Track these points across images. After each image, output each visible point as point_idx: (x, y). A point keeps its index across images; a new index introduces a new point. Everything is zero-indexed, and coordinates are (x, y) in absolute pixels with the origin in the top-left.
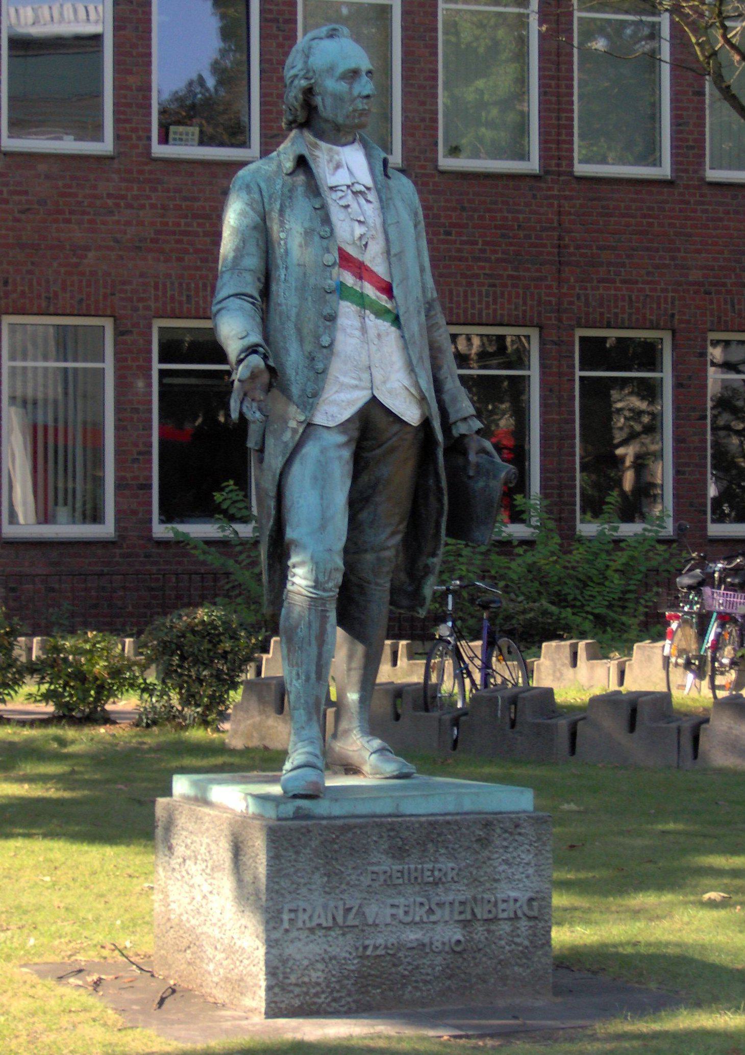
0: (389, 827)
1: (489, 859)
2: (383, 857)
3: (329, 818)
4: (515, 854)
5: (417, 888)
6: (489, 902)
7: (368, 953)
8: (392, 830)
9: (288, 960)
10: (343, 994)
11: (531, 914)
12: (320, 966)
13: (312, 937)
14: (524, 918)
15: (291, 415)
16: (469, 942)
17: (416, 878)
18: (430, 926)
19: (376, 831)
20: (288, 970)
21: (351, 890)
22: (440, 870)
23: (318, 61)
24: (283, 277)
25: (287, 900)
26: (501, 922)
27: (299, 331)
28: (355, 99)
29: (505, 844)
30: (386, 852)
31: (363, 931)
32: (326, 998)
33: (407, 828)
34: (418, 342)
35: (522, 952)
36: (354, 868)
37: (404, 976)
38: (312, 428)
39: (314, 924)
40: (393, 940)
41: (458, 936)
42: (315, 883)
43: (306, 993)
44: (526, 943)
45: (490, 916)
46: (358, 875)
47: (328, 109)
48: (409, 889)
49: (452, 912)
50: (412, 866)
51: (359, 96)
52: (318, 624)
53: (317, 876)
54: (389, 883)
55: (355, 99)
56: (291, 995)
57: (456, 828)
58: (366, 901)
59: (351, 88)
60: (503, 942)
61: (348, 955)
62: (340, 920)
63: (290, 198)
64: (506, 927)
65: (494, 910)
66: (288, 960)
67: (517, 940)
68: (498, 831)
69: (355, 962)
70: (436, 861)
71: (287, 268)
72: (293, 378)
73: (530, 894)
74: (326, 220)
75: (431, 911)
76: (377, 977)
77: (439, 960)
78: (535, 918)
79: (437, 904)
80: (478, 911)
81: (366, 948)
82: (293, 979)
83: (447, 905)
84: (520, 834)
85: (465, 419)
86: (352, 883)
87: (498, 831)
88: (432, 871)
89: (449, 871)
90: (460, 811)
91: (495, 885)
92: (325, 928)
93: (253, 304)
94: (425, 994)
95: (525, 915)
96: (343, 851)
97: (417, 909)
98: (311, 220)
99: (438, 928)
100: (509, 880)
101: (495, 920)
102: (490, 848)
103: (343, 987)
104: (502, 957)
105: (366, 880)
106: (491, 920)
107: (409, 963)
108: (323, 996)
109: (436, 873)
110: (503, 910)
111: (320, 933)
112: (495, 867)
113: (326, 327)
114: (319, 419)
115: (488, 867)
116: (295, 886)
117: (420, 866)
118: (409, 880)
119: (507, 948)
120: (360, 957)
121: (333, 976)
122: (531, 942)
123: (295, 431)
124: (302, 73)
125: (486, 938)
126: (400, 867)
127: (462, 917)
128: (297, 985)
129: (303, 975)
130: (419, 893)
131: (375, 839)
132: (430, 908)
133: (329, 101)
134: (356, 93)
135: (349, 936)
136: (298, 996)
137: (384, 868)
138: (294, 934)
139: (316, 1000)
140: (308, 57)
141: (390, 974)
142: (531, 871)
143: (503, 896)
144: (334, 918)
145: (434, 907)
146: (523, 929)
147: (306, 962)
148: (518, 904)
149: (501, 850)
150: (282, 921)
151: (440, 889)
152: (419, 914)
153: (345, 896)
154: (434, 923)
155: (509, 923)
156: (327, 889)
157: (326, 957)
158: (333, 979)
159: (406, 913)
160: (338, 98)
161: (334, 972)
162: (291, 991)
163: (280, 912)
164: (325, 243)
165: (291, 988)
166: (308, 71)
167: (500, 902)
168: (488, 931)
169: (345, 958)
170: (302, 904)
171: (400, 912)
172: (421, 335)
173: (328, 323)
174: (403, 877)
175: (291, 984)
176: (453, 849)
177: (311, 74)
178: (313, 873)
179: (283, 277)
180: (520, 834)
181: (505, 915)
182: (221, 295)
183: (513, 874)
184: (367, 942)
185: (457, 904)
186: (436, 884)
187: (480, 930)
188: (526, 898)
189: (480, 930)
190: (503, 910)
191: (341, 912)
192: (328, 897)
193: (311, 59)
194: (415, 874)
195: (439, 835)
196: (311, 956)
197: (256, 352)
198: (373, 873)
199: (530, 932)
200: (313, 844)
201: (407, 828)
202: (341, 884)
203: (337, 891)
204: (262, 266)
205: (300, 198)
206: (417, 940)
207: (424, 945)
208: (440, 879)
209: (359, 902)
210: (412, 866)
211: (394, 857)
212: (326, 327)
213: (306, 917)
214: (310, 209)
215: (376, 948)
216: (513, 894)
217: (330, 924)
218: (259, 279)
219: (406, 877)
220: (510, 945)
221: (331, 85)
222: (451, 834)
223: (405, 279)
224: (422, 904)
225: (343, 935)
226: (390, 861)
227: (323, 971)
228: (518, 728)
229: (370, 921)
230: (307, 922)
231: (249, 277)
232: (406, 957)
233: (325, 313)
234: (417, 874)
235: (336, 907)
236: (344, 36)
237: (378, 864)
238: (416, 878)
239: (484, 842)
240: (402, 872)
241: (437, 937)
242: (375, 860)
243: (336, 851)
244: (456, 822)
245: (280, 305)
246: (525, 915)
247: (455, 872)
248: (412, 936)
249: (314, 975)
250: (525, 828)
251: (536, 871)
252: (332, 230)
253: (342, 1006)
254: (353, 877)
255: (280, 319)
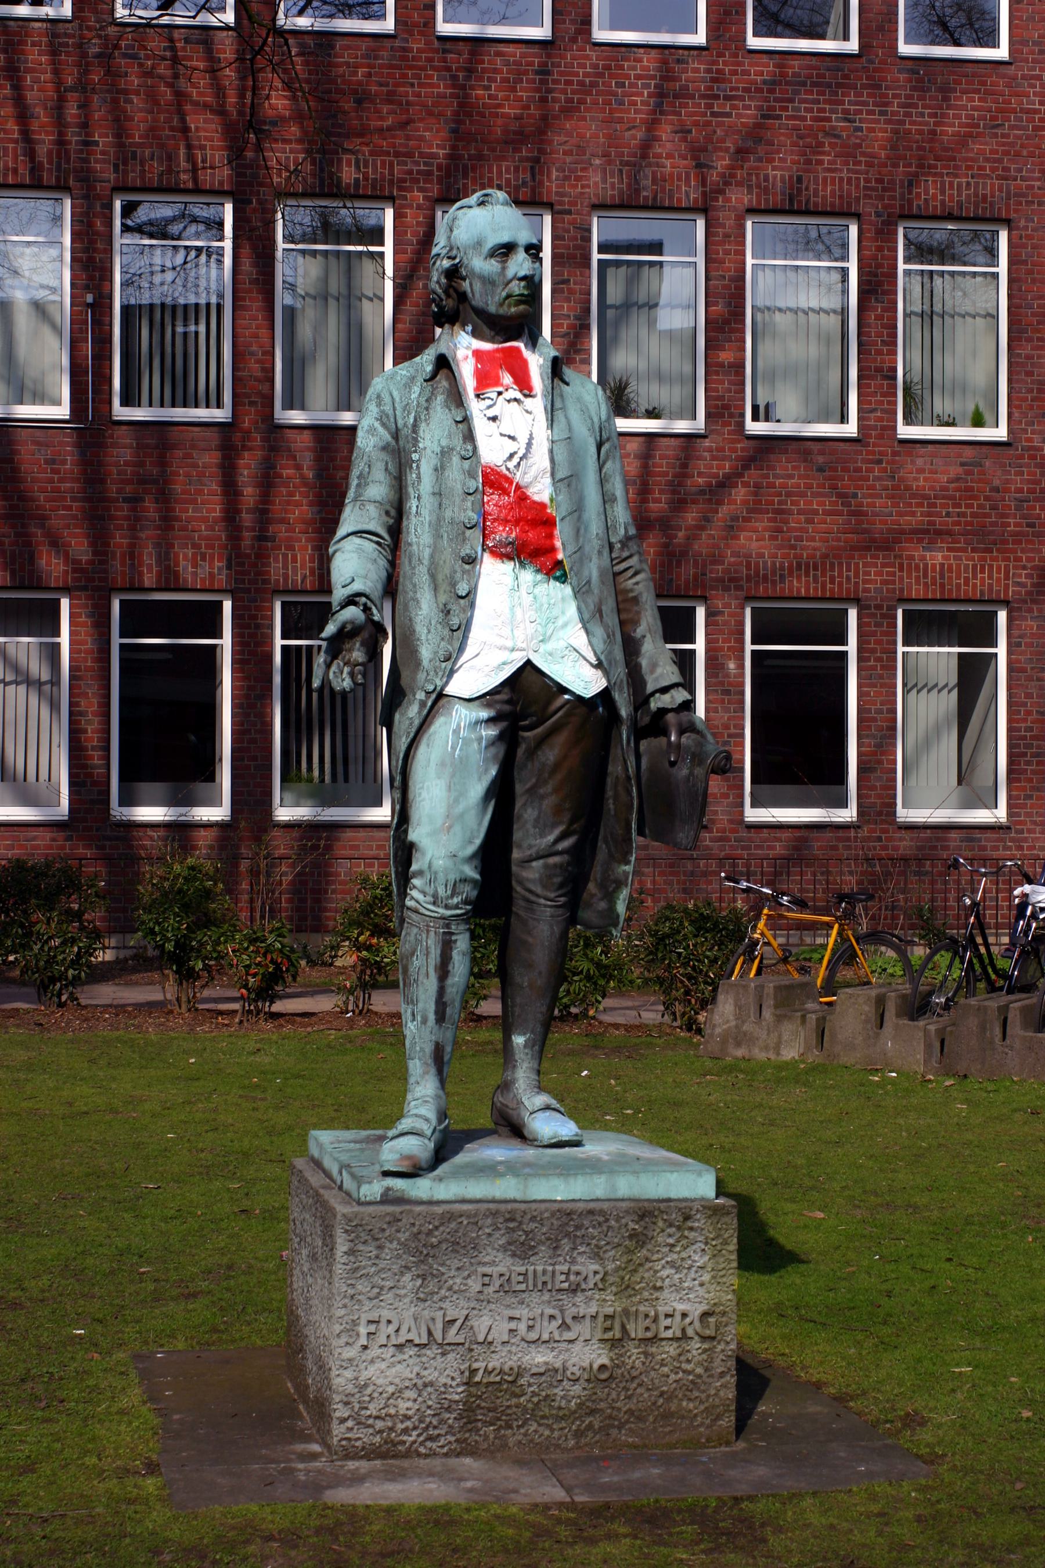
0: (507, 1216)
1: (647, 1260)
2: (500, 1255)
3: (430, 1203)
4: (684, 1255)
5: (546, 1296)
6: (647, 1316)
7: (477, 1379)
8: (512, 1220)
9: (366, 1386)
10: (443, 1432)
11: (708, 1332)
12: (412, 1394)
13: (400, 1357)
14: (696, 1338)
15: (420, 684)
16: (618, 1366)
17: (545, 1283)
18: (564, 1345)
19: (489, 1221)
20: (367, 1399)
21: (455, 1296)
22: (578, 1273)
23: (463, 234)
24: (414, 509)
25: (366, 1308)
26: (664, 1343)
27: (433, 577)
28: (511, 281)
29: (671, 1241)
30: (504, 1248)
31: (471, 1350)
32: (419, 1435)
33: (533, 1219)
34: (596, 591)
35: (692, 1382)
36: (458, 1269)
37: (525, 1410)
38: (444, 701)
39: (401, 1340)
40: (511, 1363)
41: (604, 1360)
42: (404, 1287)
43: (391, 1429)
44: (699, 1370)
45: (649, 1335)
46: (466, 1278)
47: (477, 295)
48: (535, 1298)
49: (593, 1329)
50: (540, 1268)
51: (515, 278)
52: (439, 952)
53: (408, 1277)
54: (506, 1289)
55: (511, 281)
56: (371, 1431)
57: (601, 1219)
58: (475, 1312)
59: (504, 269)
60: (666, 1369)
61: (449, 1382)
62: (438, 1335)
63: (427, 409)
64: (672, 1349)
65: (653, 1327)
66: (366, 1386)
67: (686, 1366)
68: (661, 1224)
69: (460, 1390)
70: (573, 1262)
71: (419, 498)
72: (423, 637)
73: (703, 1308)
74: (469, 436)
75: (565, 1326)
76: (489, 1410)
77: (577, 1389)
78: (713, 1338)
79: (574, 1318)
80: (630, 1327)
81: (473, 1372)
82: (373, 1409)
83: (588, 1320)
84: (691, 1229)
85: (664, 690)
86: (456, 1288)
87: (661, 1224)
88: (568, 1274)
89: (591, 1275)
90: (613, 1196)
91: (656, 1295)
92: (417, 1345)
93: (378, 543)
94: (556, 1434)
95: (697, 1334)
96: (444, 1246)
97: (545, 1323)
98: (450, 436)
99: (577, 1348)
100: (677, 1288)
101: (655, 1339)
102: (649, 1246)
103: (442, 1422)
104: (665, 1388)
105: (475, 1285)
106: (649, 1339)
107: (534, 1393)
108: (415, 1433)
109: (572, 1277)
110: (667, 1328)
111: (411, 1351)
112: (656, 1272)
113: (464, 572)
114: (449, 690)
115: (648, 1270)
116: (376, 1290)
117: (550, 1268)
118: (535, 1285)
119: (673, 1377)
120: (466, 1384)
121: (429, 1407)
122: (706, 1370)
123: (423, 704)
124: (444, 251)
125: (644, 1363)
126: (523, 1269)
127: (609, 1335)
128: (377, 1418)
129: (386, 1406)
130: (549, 1302)
131: (487, 1231)
132: (564, 1323)
133: (478, 286)
134: (510, 273)
135: (451, 1356)
136: (380, 1432)
137: (501, 1269)
138: (374, 1352)
139: (405, 1438)
140: (451, 231)
141: (508, 1407)
142: (706, 1277)
143: (668, 1309)
144: (430, 1333)
145: (569, 1321)
146: (694, 1352)
147: (391, 1389)
148: (688, 1320)
149: (666, 1249)
150: (358, 1335)
151: (579, 1298)
152: (549, 1329)
153: (446, 1305)
154: (570, 1342)
155: (675, 1345)
156: (422, 1296)
157: (420, 1382)
158: (429, 1412)
159: (530, 1328)
160: (488, 282)
161: (430, 1403)
162: (369, 1426)
163: (355, 1323)
164: (466, 464)
165: (370, 1421)
166: (451, 249)
167: (662, 1317)
168: (646, 1354)
169: (445, 1385)
170: (386, 1314)
171: (522, 1327)
172: (603, 583)
173: (467, 567)
174: (526, 1281)
175: (370, 1416)
176: (596, 1246)
177: (454, 252)
178: (402, 1274)
179: (414, 509)
180: (691, 1229)
181: (669, 1334)
182: (341, 532)
183: (681, 1281)
184: (475, 1365)
185: (601, 1319)
186: (574, 1291)
187: (634, 1354)
188: (698, 1313)
189: (634, 1354)
190: (667, 1328)
191: (439, 1325)
192: (422, 1305)
193: (455, 232)
194: (544, 1279)
195: (578, 1227)
196: (397, 1381)
197: (355, 604)
198: (485, 1275)
199: (705, 1356)
200: (403, 1237)
201: (533, 1219)
202: (440, 1288)
203: (436, 1298)
204: (393, 496)
205: (439, 408)
206: (546, 1363)
207: (556, 1371)
208: (578, 1285)
209: (465, 1312)
210: (540, 1268)
211: (514, 1255)
212: (464, 572)
213: (391, 1329)
214: (450, 422)
215: (488, 1372)
216: (681, 1307)
217: (424, 1341)
218: (387, 513)
219: (531, 1282)
220: (677, 1373)
221: (481, 264)
222: (594, 1227)
223: (578, 509)
224: (552, 1317)
225: (443, 1354)
226: (509, 1261)
227: (415, 1400)
228: (1008, 1042)
229: (481, 1339)
230: (393, 1337)
231: (372, 510)
232: (530, 1385)
233: (463, 554)
234: (547, 1278)
235: (433, 1319)
236: (497, 203)
237: (493, 1263)
238: (545, 1283)
239: (640, 1239)
240: (525, 1275)
241: (573, 1360)
242: (486, 1259)
243: (433, 1246)
244: (602, 1213)
245: (410, 545)
246: (697, 1334)
247: (599, 1277)
248: (539, 1358)
249: (403, 1406)
250: (698, 1220)
251: (713, 1277)
252: (475, 449)
253: (442, 1447)
254: (458, 1281)
255: (410, 562)
